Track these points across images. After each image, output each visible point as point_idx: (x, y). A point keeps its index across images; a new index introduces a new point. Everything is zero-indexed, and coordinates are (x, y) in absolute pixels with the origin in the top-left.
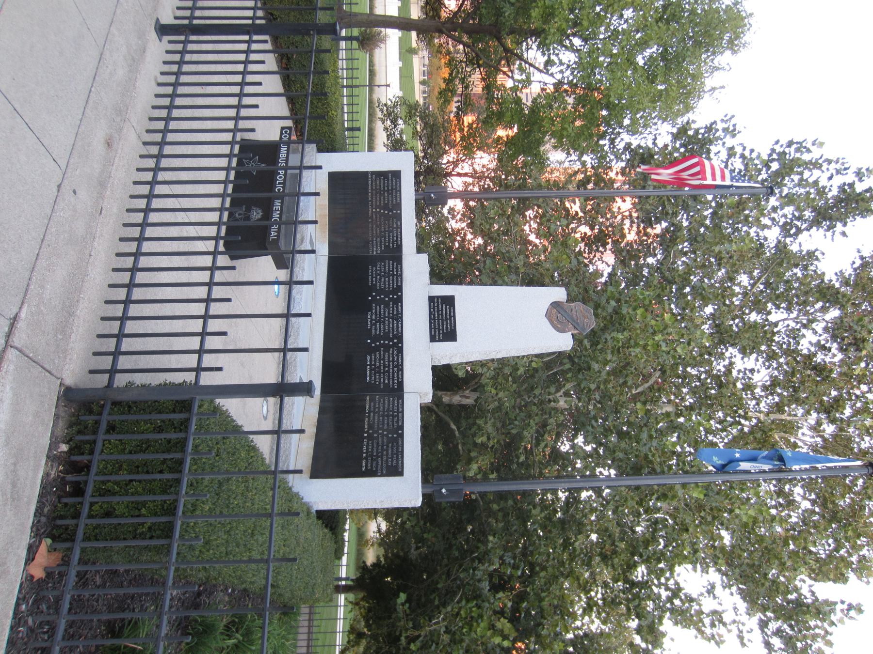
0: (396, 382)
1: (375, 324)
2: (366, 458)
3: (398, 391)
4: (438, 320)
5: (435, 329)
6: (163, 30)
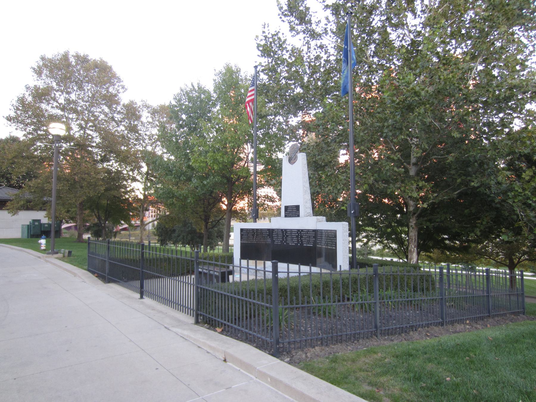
6: (142, 297)
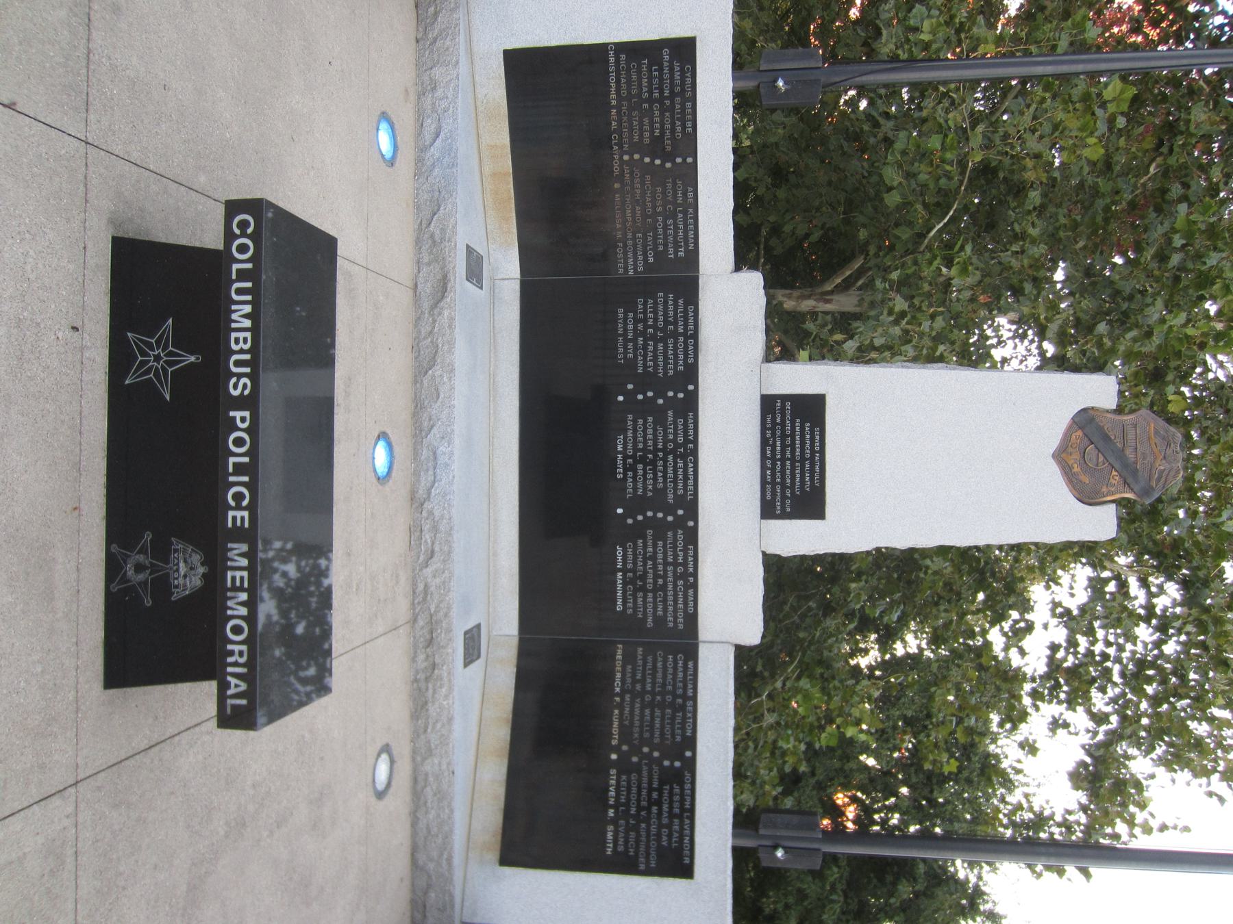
0: (680, 614)
2: (614, 822)
3: (684, 642)
4: (783, 460)
5: (773, 483)
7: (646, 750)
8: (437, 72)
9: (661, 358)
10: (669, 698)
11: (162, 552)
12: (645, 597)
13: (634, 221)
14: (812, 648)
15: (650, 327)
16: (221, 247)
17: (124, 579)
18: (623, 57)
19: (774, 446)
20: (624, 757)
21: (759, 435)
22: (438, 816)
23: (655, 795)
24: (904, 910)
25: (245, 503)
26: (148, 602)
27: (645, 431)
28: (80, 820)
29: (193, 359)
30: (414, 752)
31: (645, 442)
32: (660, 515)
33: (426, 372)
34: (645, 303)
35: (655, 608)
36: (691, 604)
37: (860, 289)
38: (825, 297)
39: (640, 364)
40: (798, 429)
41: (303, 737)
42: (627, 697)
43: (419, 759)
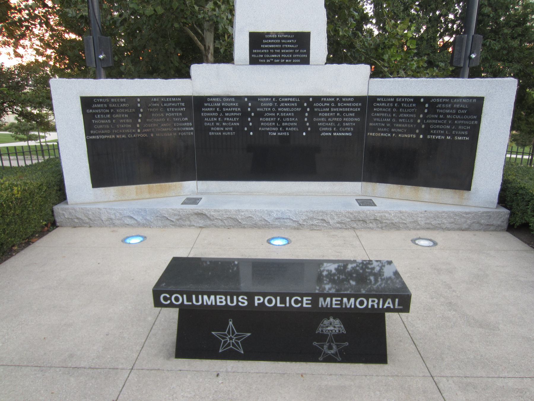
0: (354, 105)
1: (284, 127)
2: (453, 136)
3: (367, 103)
4: (281, 53)
7: (419, 121)
8: (104, 218)
9: (232, 114)
10: (394, 110)
11: (323, 337)
12: (346, 122)
13: (168, 127)
14: (369, 53)
15: (218, 119)
16: (178, 309)
17: (336, 354)
18: (92, 132)
19: (274, 58)
20: (422, 132)
21: (269, 66)
22: (445, 218)
23: (441, 116)
24: (496, 10)
25: (299, 299)
26: (347, 344)
27: (267, 122)
28: (450, 375)
29: (231, 323)
30: (415, 229)
31: (272, 122)
32: (307, 114)
33: (240, 223)
34: (207, 122)
35: (351, 117)
36: (349, 99)
37: (202, 30)
38: (207, 50)
39: (235, 124)
40: (266, 46)
41: (408, 277)
42: (393, 130)
43: (418, 227)
